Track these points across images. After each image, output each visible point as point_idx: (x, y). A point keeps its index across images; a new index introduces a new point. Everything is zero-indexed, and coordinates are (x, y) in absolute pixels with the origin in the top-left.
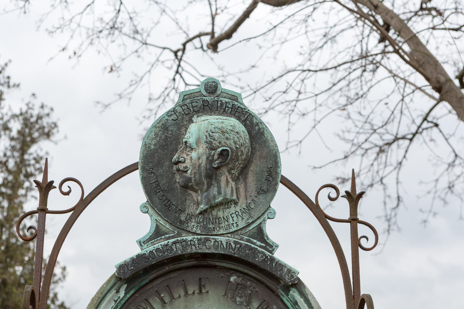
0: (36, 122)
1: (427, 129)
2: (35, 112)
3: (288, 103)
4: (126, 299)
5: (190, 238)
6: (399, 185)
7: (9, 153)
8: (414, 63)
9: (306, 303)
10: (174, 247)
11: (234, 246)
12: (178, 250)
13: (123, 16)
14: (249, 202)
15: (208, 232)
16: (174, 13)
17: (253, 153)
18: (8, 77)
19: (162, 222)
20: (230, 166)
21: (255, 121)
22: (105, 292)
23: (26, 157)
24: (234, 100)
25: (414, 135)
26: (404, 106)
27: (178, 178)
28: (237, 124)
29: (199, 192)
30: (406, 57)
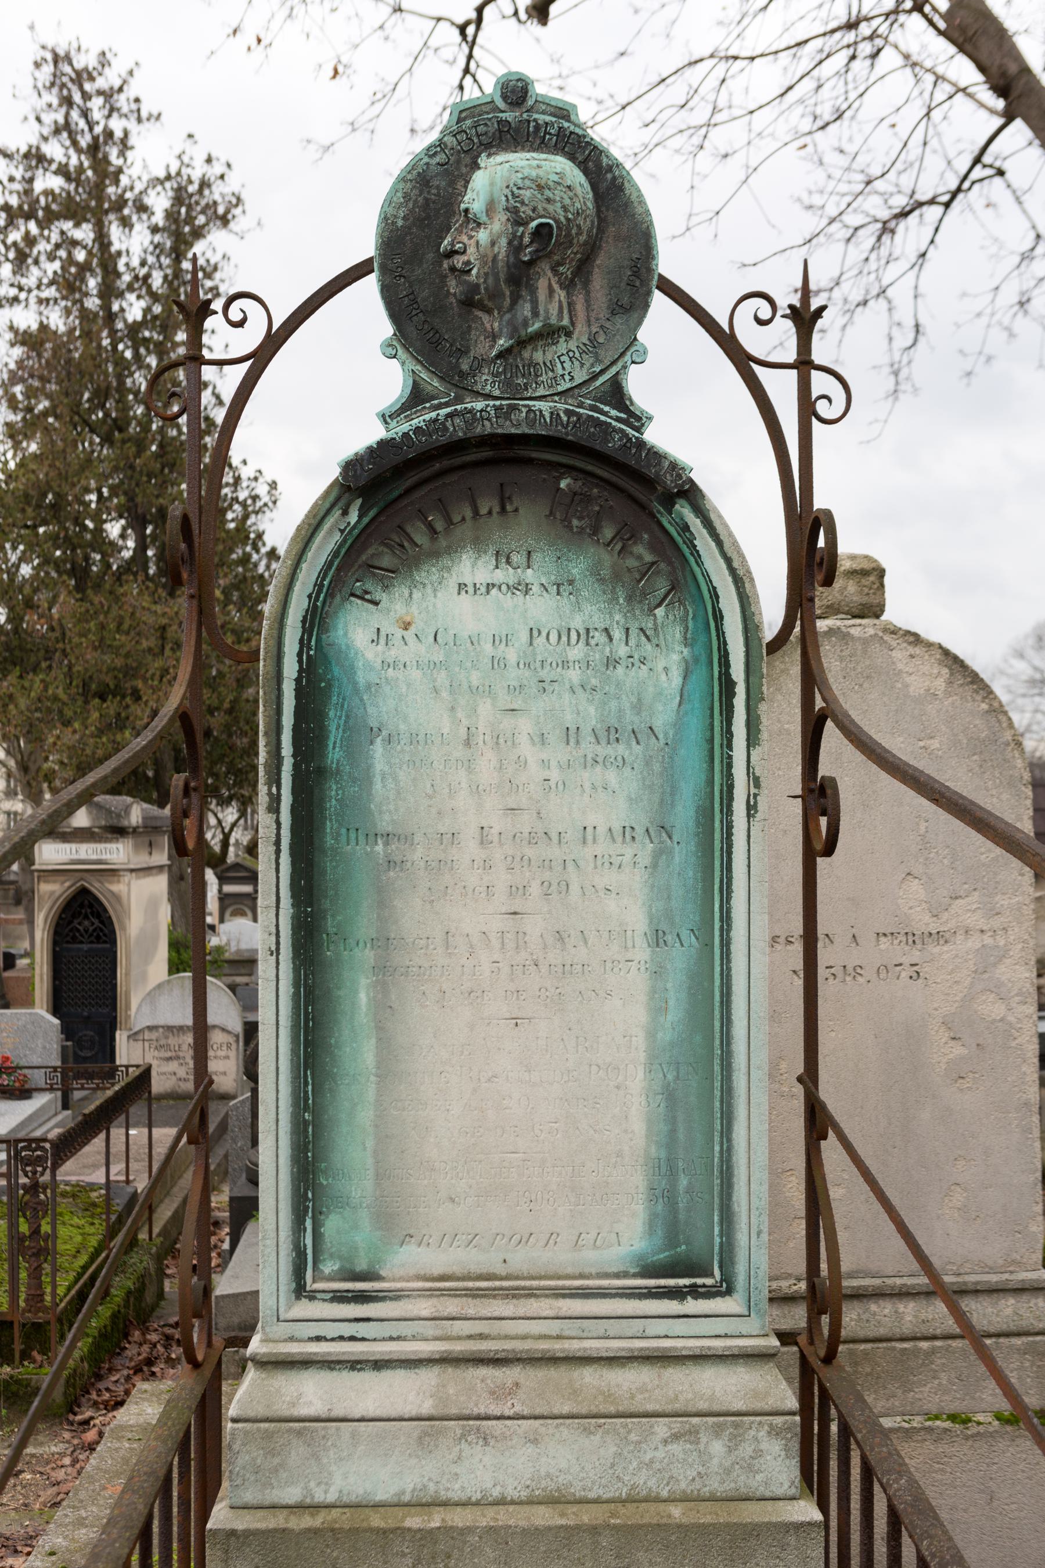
1: (981, 180)
2: (196, 175)
3: (692, 131)
4: (361, 526)
5: (479, 405)
6: (919, 300)
7: (151, 260)
8: (955, 35)
9: (705, 527)
10: (449, 424)
11: (565, 419)
12: (457, 429)
14: (594, 330)
15: (514, 392)
17: (601, 230)
18: (137, 100)
19: (424, 375)
20: (556, 258)
21: (605, 161)
22: (322, 514)
24: (563, 118)
25: (954, 194)
26: (931, 132)
27: (453, 286)
28: (568, 168)
29: (496, 313)
30: (937, 19)
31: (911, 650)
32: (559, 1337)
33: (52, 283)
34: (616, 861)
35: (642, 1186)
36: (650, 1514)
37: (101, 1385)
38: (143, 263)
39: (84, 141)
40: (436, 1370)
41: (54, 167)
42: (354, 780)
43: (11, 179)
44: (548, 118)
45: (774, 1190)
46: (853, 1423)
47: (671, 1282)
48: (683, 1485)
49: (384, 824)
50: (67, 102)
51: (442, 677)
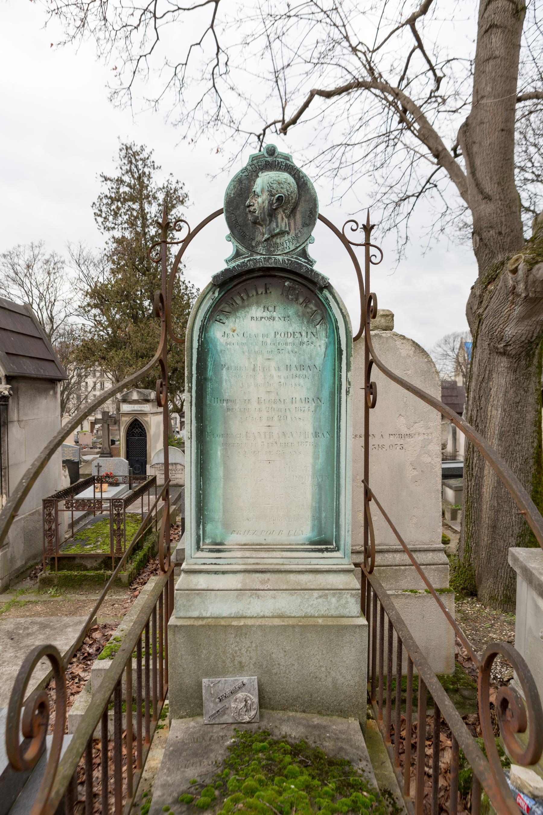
0: (174, 193)
2: (173, 187)
5: (258, 257)
7: (158, 215)
8: (421, 137)
12: (251, 265)
13: (223, 110)
15: (270, 253)
16: (258, 106)
17: (299, 198)
18: (153, 162)
21: (301, 175)
25: (420, 194)
27: (250, 217)
30: (415, 132)
31: (402, 341)
32: (282, 564)
33: (125, 223)
34: (303, 409)
35: (310, 516)
36: (311, 621)
37: (140, 577)
38: (155, 216)
39: (136, 175)
40: (243, 574)
41: (126, 184)
42: (217, 382)
43: (112, 188)
44: (282, 160)
45: (354, 517)
46: (378, 593)
47: (319, 547)
48: (322, 612)
49: (226, 396)
50: (131, 162)
51: (245, 348)
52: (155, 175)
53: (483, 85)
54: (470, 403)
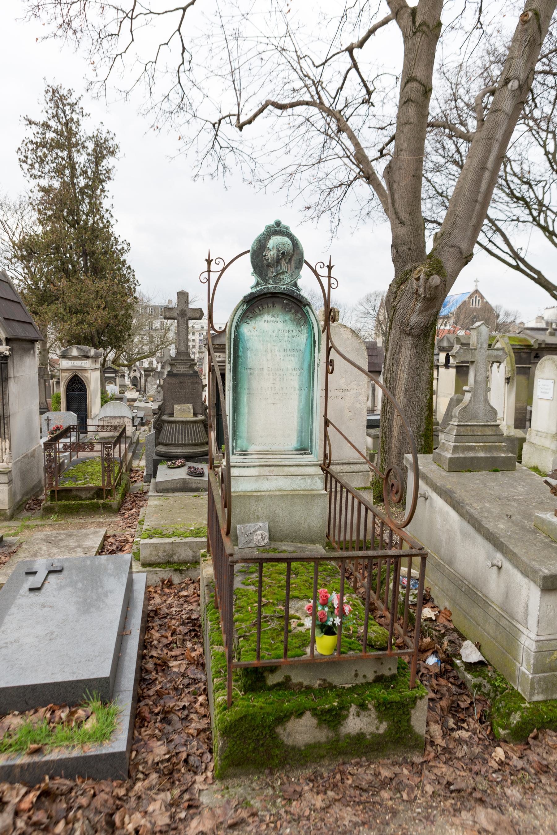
2: (103, 136)
5: (270, 286)
7: (87, 165)
12: (265, 291)
15: (276, 283)
18: (82, 108)
23: (100, 168)
27: (265, 262)
36: (297, 492)
38: (84, 167)
39: (64, 121)
41: (53, 129)
49: (250, 366)
50: (57, 106)
52: (84, 122)
53: (402, 142)
54: (386, 368)
